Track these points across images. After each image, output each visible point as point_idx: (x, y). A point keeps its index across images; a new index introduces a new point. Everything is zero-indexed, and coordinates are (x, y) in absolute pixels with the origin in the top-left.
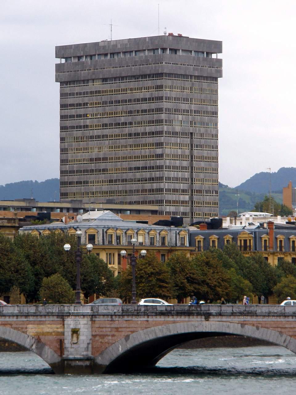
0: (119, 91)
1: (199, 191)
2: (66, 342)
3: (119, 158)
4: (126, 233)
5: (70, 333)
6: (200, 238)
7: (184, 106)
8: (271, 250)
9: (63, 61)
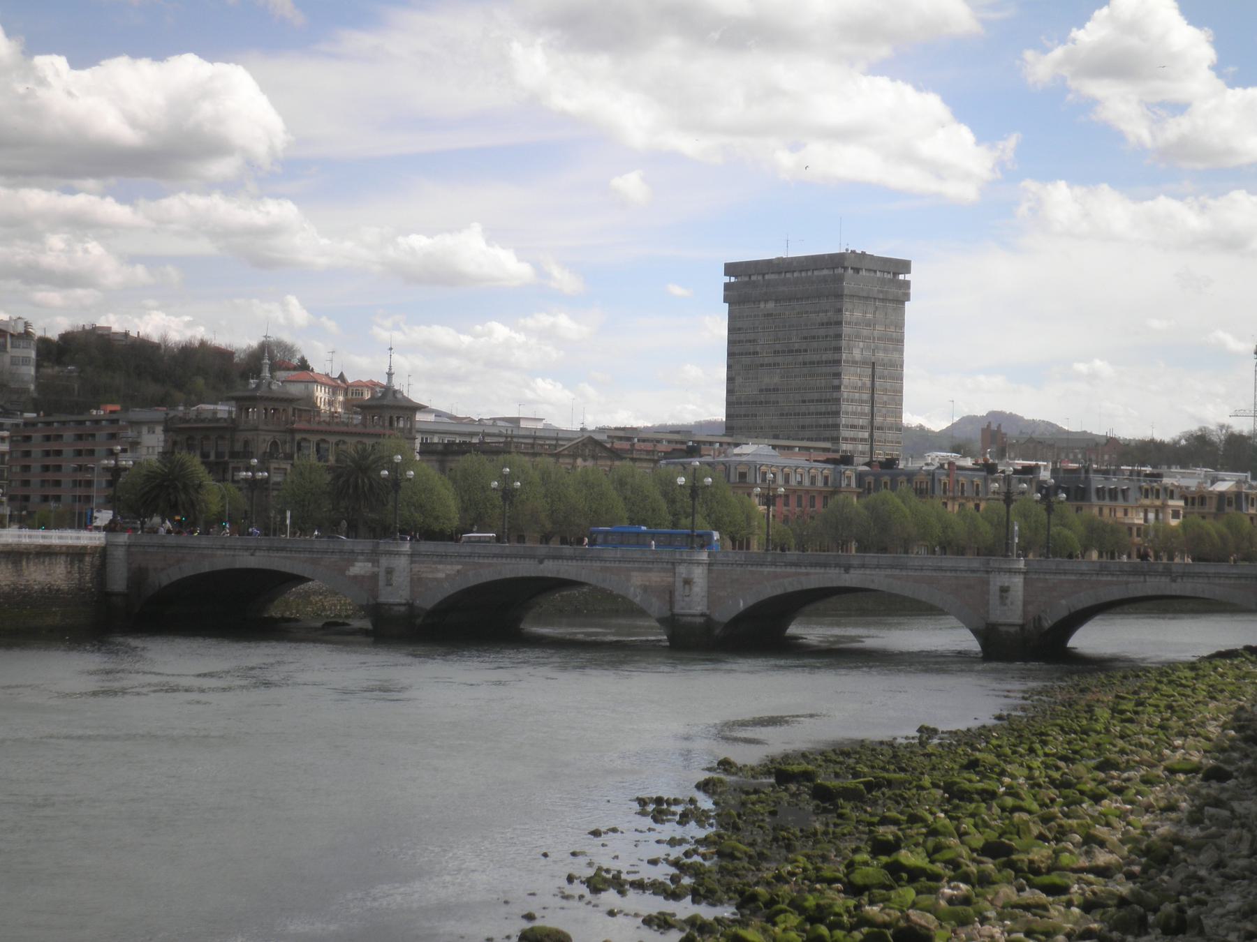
2: (677, 593)
4: (782, 470)
5: (682, 584)
6: (870, 479)
8: (951, 494)
9: (733, 279)
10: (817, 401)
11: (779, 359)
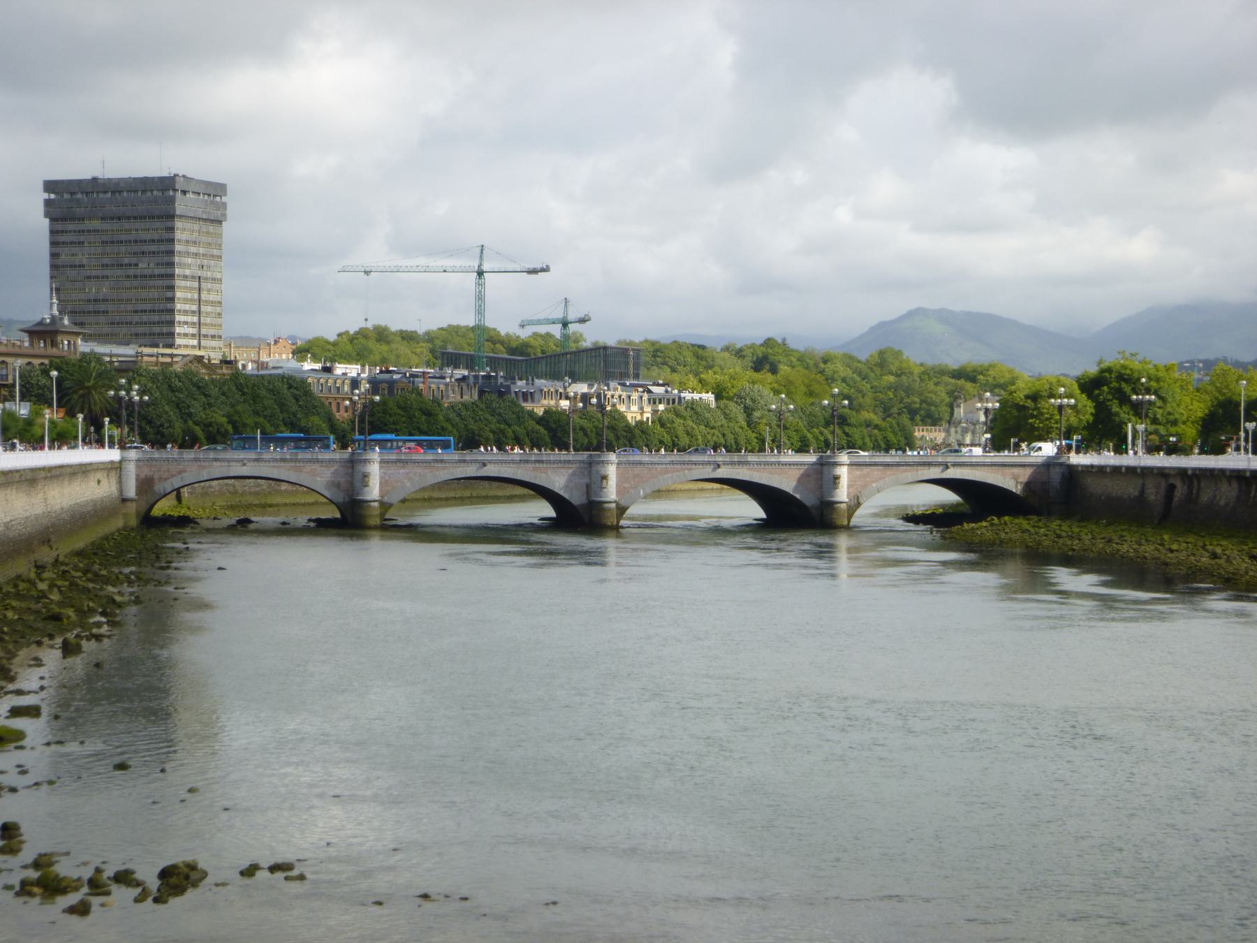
0: (121, 230)
1: (205, 336)
3: (122, 300)
4: (318, 381)
7: (193, 249)
9: (53, 196)
10: (150, 311)
11: (108, 272)
